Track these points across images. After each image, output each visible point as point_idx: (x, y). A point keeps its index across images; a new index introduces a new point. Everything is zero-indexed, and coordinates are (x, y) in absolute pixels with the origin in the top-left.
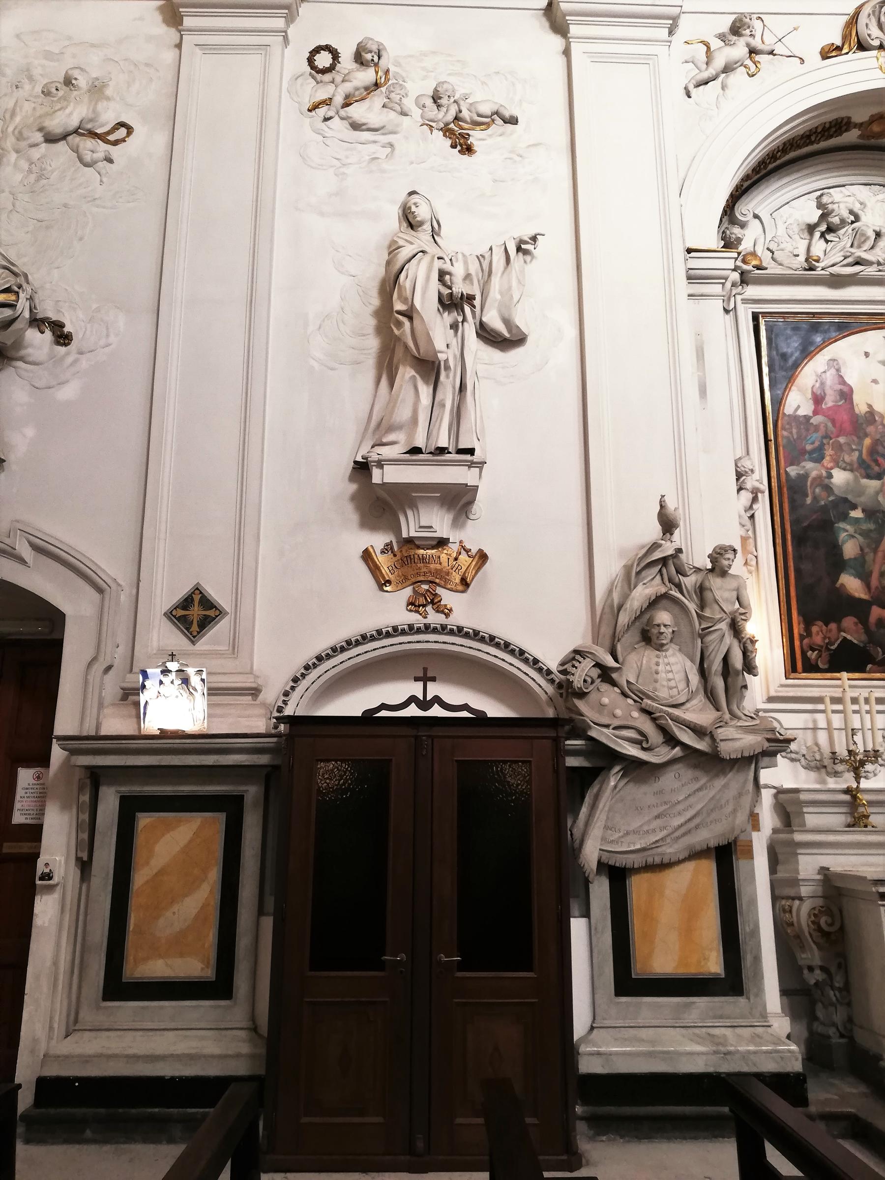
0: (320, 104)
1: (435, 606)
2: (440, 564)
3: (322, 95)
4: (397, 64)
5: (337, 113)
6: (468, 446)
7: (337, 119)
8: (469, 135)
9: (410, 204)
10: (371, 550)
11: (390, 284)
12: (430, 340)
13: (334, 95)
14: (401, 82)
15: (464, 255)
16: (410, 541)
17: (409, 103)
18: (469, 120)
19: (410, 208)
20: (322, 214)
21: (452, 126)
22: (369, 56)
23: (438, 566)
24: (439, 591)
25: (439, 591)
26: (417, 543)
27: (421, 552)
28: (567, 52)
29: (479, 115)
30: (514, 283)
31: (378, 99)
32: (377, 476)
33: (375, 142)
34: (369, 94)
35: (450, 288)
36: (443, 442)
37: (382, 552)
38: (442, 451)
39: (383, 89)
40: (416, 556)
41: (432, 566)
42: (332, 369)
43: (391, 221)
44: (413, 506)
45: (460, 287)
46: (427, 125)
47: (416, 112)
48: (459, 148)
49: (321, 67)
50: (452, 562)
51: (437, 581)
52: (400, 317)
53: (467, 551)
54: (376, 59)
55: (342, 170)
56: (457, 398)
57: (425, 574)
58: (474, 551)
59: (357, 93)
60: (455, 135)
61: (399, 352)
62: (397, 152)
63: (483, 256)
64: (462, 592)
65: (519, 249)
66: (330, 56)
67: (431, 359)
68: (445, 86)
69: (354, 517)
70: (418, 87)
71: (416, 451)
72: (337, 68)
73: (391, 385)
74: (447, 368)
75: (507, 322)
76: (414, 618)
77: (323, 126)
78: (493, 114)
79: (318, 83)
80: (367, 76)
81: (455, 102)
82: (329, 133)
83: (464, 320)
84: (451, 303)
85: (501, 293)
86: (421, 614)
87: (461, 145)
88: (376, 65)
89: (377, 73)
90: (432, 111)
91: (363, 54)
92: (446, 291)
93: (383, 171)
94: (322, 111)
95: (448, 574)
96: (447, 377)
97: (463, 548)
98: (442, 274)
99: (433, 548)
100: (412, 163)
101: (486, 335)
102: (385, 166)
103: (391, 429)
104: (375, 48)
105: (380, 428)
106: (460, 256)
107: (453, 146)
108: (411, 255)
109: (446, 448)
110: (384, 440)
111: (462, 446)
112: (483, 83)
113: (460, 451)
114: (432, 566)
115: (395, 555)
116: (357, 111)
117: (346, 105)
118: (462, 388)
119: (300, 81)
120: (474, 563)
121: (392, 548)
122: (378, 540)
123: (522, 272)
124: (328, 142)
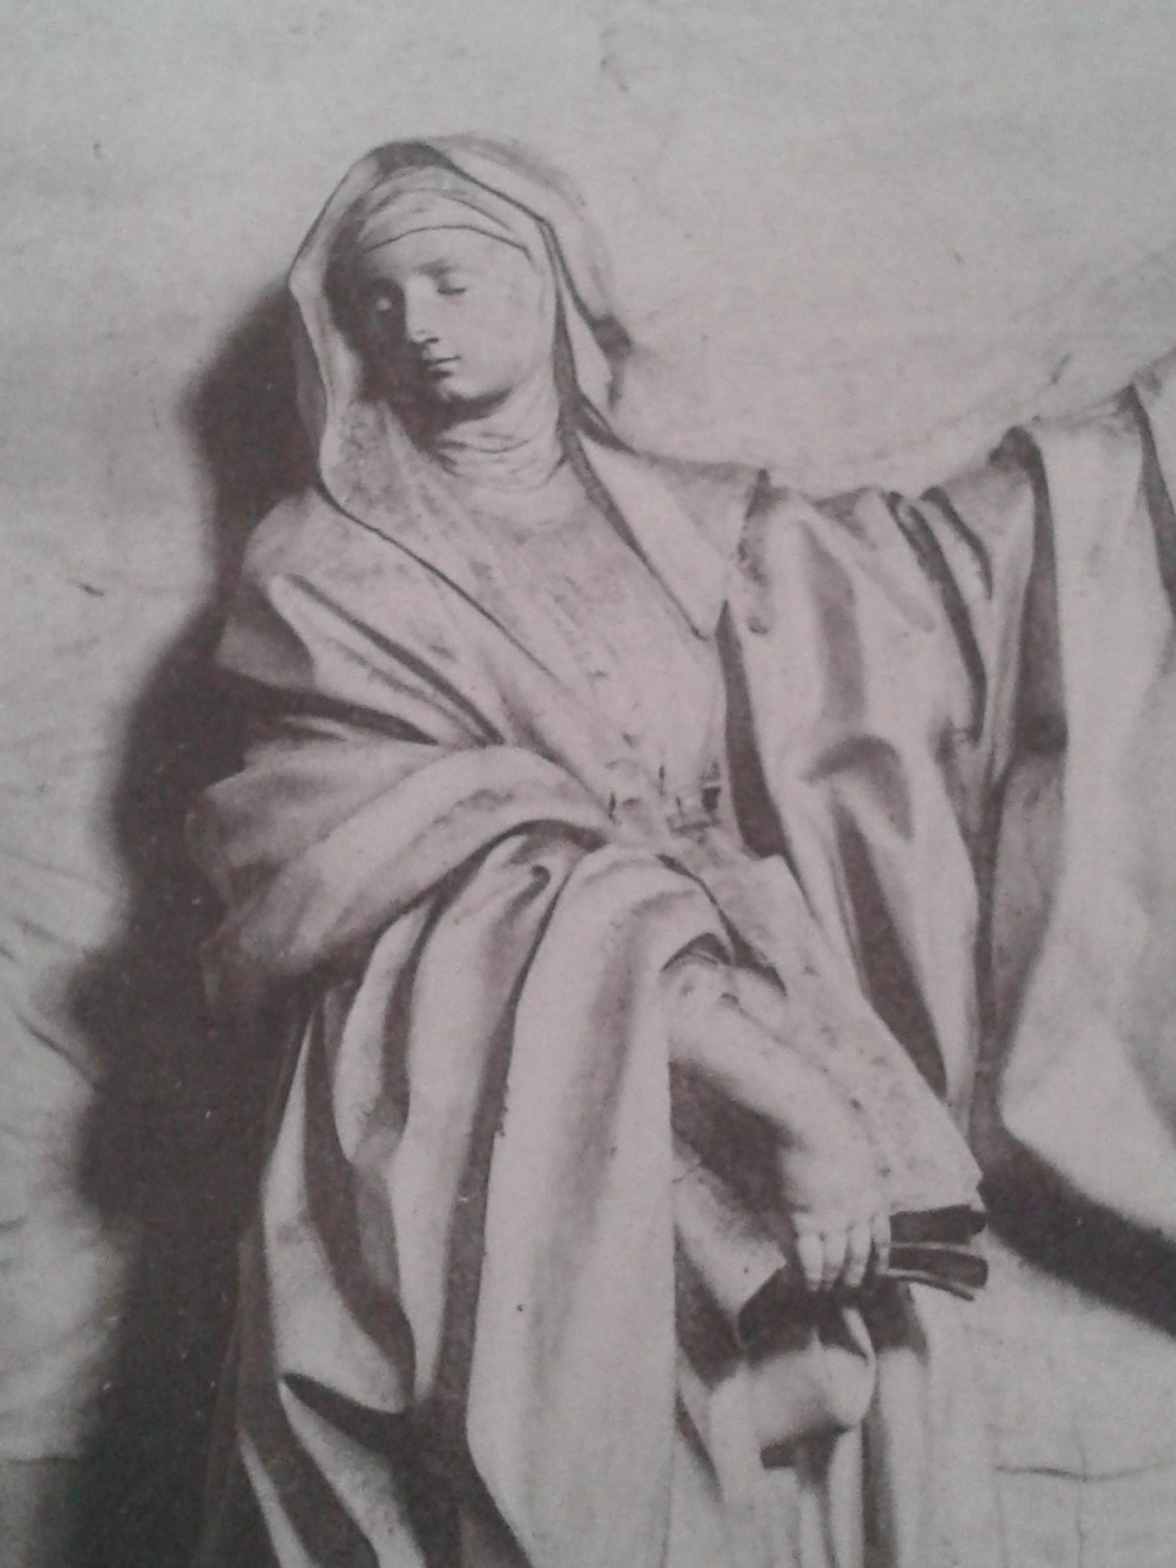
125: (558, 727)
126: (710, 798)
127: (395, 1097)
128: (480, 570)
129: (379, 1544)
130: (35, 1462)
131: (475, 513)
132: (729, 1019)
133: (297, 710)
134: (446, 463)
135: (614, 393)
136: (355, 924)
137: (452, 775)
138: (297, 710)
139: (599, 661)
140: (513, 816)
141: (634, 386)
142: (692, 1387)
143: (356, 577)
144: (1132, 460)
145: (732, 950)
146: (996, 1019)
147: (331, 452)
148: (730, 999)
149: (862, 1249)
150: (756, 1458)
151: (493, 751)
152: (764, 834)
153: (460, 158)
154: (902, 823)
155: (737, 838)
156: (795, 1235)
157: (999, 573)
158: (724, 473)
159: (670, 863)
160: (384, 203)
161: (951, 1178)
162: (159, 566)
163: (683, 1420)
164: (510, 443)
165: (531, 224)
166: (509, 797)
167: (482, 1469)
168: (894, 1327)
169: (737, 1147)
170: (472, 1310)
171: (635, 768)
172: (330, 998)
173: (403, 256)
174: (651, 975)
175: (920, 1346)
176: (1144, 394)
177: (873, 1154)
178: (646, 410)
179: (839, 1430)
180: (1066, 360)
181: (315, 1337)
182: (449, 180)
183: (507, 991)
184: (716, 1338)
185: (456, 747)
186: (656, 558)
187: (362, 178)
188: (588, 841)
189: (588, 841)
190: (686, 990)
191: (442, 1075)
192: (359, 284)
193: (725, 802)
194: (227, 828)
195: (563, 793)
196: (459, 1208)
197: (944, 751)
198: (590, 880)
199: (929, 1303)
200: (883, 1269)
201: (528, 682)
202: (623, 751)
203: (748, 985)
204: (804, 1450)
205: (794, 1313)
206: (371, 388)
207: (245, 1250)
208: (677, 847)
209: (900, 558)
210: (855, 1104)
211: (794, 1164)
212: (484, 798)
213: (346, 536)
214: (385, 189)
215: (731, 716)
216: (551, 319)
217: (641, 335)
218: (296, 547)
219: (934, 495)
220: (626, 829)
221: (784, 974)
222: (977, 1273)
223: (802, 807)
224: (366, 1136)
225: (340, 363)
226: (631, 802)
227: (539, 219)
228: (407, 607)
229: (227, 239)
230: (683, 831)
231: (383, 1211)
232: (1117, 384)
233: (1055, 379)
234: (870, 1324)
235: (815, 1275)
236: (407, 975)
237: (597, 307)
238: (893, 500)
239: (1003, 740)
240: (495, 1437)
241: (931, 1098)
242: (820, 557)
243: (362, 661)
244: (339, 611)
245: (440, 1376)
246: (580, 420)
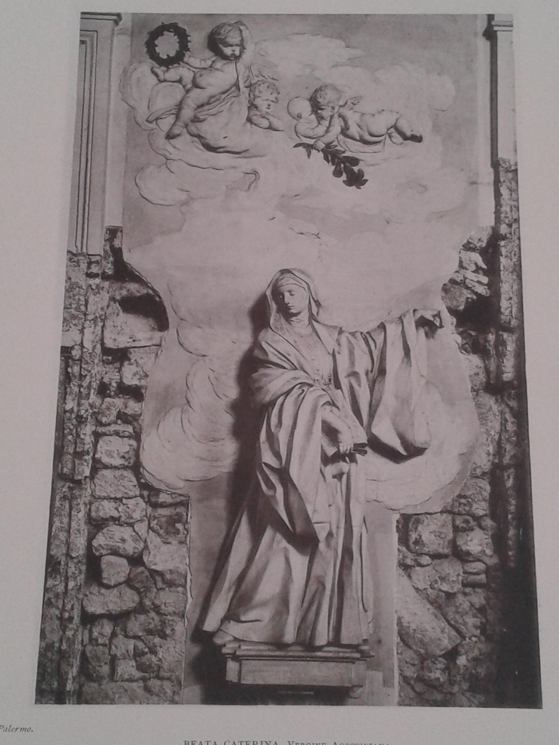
5: (186, 126)
18: (358, 138)
22: (228, 51)
29: (371, 135)
107: (337, 173)
125: (307, 367)
126: (330, 380)
127: (280, 423)
128: (295, 342)
129: (276, 486)
130: (227, 472)
131: (294, 332)
132: (331, 414)
133: (266, 363)
134: (290, 324)
135: (318, 313)
136: (274, 397)
137: (290, 374)
138: (266, 363)
139: (313, 358)
140: (299, 381)
141: (321, 312)
142: (323, 466)
143: (276, 342)
144: (400, 328)
145: (332, 404)
146: (372, 415)
147: (272, 321)
148: (331, 411)
149: (349, 448)
150: (331, 477)
151: (296, 371)
152: (338, 386)
153: (294, 272)
154: (360, 386)
155: (334, 386)
156: (339, 446)
157: (377, 346)
158: (335, 327)
159: (324, 390)
160: (282, 279)
161: (363, 439)
162: (245, 339)
163: (321, 471)
164: (300, 321)
165: (305, 284)
166: (299, 378)
167: (292, 476)
168: (353, 459)
169: (331, 433)
170: (291, 455)
171: (318, 375)
172: (270, 408)
173: (284, 289)
174: (319, 407)
175: (357, 463)
176: (403, 318)
177: (351, 434)
178: (323, 316)
179: (343, 473)
180: (391, 311)
181: (267, 457)
182: (292, 276)
183: (297, 408)
184: (327, 460)
185: (291, 370)
186: (323, 341)
187: (278, 275)
188: (311, 386)
189: (311, 386)
190: (325, 409)
191: (287, 421)
192: (277, 292)
193: (332, 381)
194: (256, 381)
195: (307, 378)
196: (289, 440)
197: (367, 374)
198: (311, 392)
199: (358, 456)
200: (352, 452)
201: (302, 360)
202: (317, 372)
203: (334, 408)
204: (339, 476)
205: (338, 457)
206: (278, 311)
207: (257, 445)
208: (324, 387)
209: (362, 343)
210: (349, 428)
211: (340, 436)
212: (295, 378)
213: (274, 335)
214: (282, 277)
215: (334, 367)
216: (308, 301)
217: (322, 304)
218: (266, 336)
219: (368, 333)
220: (317, 384)
221: (340, 407)
222: (366, 452)
223: (344, 382)
224: (275, 429)
225: (274, 306)
226: (317, 380)
227: (307, 283)
228: (283, 347)
229: (257, 284)
230: (325, 385)
231: (278, 440)
232: (399, 316)
233: (389, 314)
234: (349, 459)
235: (342, 452)
236: (282, 404)
237: (316, 300)
238: (362, 333)
239: (376, 372)
240: (294, 472)
241: (361, 427)
242: (350, 342)
243: (276, 355)
244: (272, 347)
245: (286, 463)
246: (312, 318)
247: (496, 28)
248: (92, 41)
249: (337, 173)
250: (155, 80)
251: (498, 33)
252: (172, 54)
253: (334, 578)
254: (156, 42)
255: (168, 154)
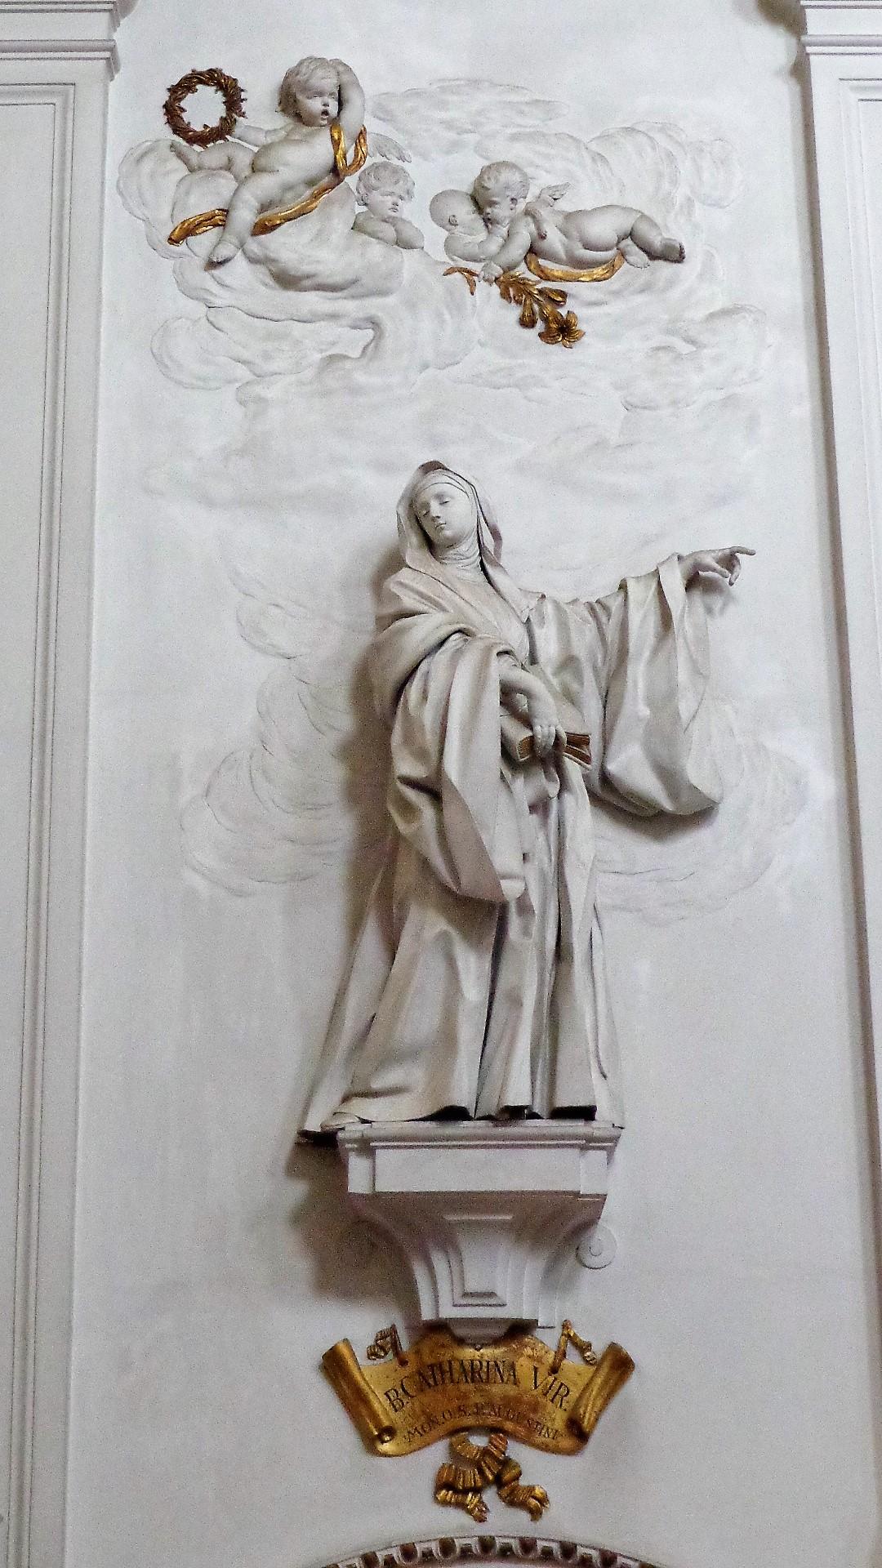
0: (199, 224)
1: (506, 1490)
2: (516, 1382)
3: (201, 203)
4: (385, 114)
5: (241, 245)
6: (582, 1102)
7: (240, 264)
8: (563, 295)
9: (428, 495)
10: (344, 1351)
11: (380, 699)
12: (482, 855)
13: (231, 204)
14: (395, 162)
15: (557, 606)
16: (439, 1327)
17: (415, 214)
18: (562, 254)
19: (427, 505)
20: (209, 502)
21: (522, 271)
22: (316, 105)
23: (511, 1390)
24: (517, 1452)
25: (517, 1452)
26: (460, 1332)
27: (468, 1353)
28: (800, 71)
29: (587, 247)
30: (683, 675)
31: (339, 211)
32: (358, 1177)
33: (333, 317)
34: (316, 197)
35: (530, 726)
36: (518, 1094)
37: (372, 1354)
38: (515, 1114)
39: (351, 181)
40: (456, 1365)
41: (497, 1390)
42: (239, 893)
43: (383, 521)
44: (447, 1241)
45: (552, 721)
46: (462, 270)
47: (433, 237)
48: (540, 326)
49: (198, 127)
50: (545, 1378)
51: (509, 1426)
52: (411, 794)
53: (583, 1348)
54: (333, 108)
55: (258, 390)
56: (549, 979)
57: (479, 1409)
58: (598, 1348)
59: (289, 195)
60: (530, 294)
61: (407, 875)
62: (388, 342)
63: (605, 608)
64: (571, 1452)
65: (694, 582)
66: (219, 97)
67: (487, 897)
68: (506, 176)
69: (301, 1266)
70: (435, 171)
71: (452, 1114)
72: (237, 130)
73: (392, 947)
74: (524, 907)
75: (668, 775)
76: (454, 1523)
77: (206, 280)
78: (621, 239)
79: (192, 170)
80: (316, 152)
81: (527, 213)
82: (222, 298)
83: (564, 786)
84: (532, 757)
85: (650, 702)
86: (470, 1512)
87: (546, 320)
88: (334, 123)
89: (336, 143)
90: (474, 235)
91: (300, 97)
92: (519, 734)
93: (355, 390)
94: (204, 241)
95: (535, 1407)
96: (526, 932)
97: (572, 1340)
98: (508, 693)
99: (496, 1342)
100: (426, 366)
101: (611, 798)
102: (360, 378)
103: (391, 1057)
104: (329, 83)
105: (358, 1046)
106: (549, 608)
107: (527, 322)
108: (433, 640)
109: (522, 1108)
110: (376, 1085)
111: (564, 1101)
112: (599, 158)
113: (560, 1114)
114: (497, 1390)
115: (403, 1363)
116: (288, 244)
117: (263, 228)
118: (562, 953)
119: (147, 166)
120: (599, 1381)
121: (395, 1345)
122: (358, 1325)
123: (702, 641)
124: (221, 320)
247: (809, 49)
248: (66, 102)
249: (527, 322)
250: (183, 170)
251: (812, 58)
252: (214, 123)
253: (539, 1001)
254: (182, 104)
255: (211, 298)
